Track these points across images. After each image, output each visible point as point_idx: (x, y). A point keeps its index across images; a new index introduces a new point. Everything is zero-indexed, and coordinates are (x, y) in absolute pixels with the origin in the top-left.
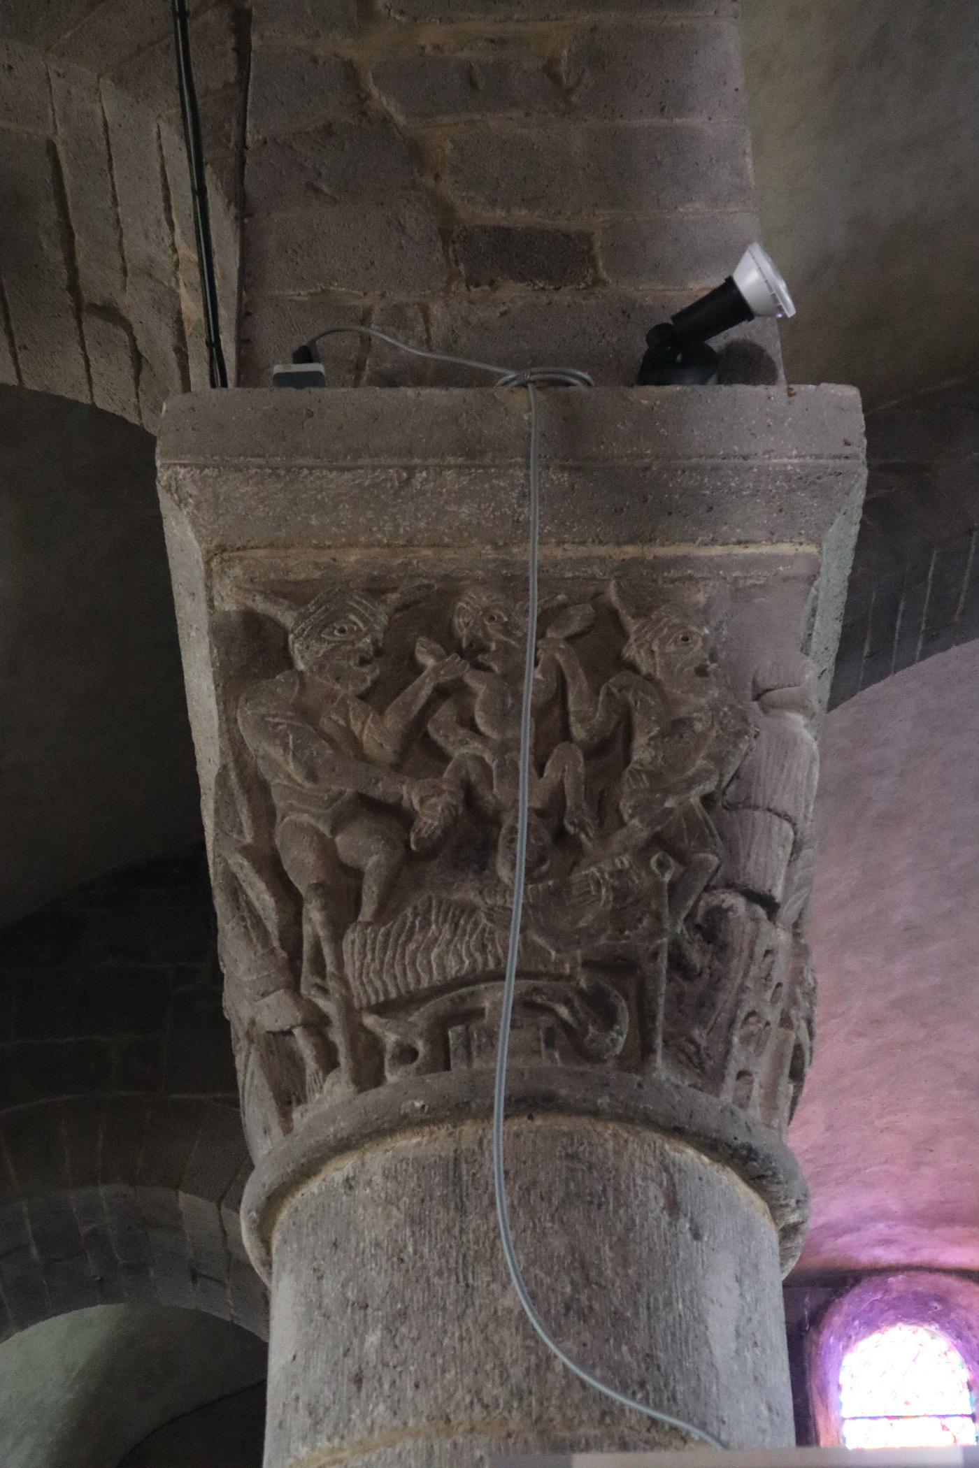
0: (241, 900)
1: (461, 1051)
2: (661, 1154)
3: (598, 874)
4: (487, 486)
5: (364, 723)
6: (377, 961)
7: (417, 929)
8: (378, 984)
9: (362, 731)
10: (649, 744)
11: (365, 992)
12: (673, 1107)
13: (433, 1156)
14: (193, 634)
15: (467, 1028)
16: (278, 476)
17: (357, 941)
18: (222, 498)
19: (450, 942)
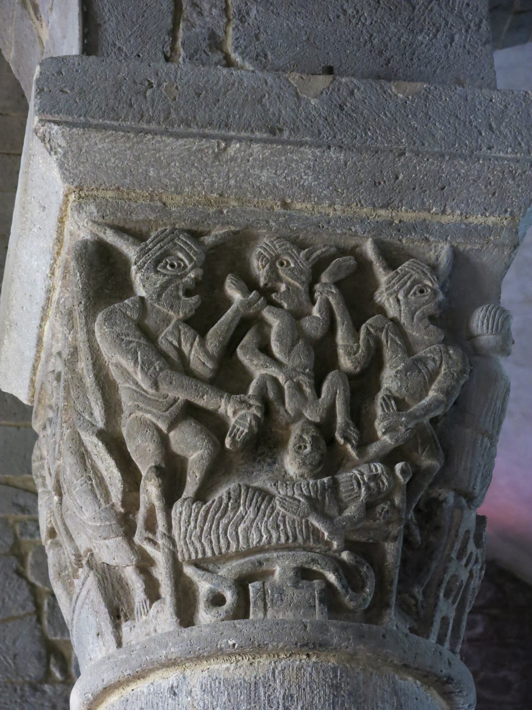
0: (87, 463)
1: (260, 603)
2: (393, 682)
3: (359, 476)
4: (283, 158)
5: (192, 345)
6: (198, 529)
7: (229, 509)
8: (198, 545)
9: (190, 351)
10: (396, 376)
11: (188, 550)
12: (405, 652)
13: (239, 679)
14: (35, 230)
15: (263, 583)
16: (129, 138)
17: (184, 513)
18: (84, 151)
19: (253, 521)
